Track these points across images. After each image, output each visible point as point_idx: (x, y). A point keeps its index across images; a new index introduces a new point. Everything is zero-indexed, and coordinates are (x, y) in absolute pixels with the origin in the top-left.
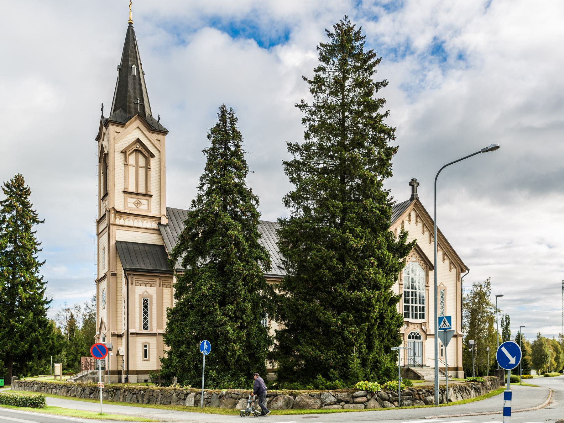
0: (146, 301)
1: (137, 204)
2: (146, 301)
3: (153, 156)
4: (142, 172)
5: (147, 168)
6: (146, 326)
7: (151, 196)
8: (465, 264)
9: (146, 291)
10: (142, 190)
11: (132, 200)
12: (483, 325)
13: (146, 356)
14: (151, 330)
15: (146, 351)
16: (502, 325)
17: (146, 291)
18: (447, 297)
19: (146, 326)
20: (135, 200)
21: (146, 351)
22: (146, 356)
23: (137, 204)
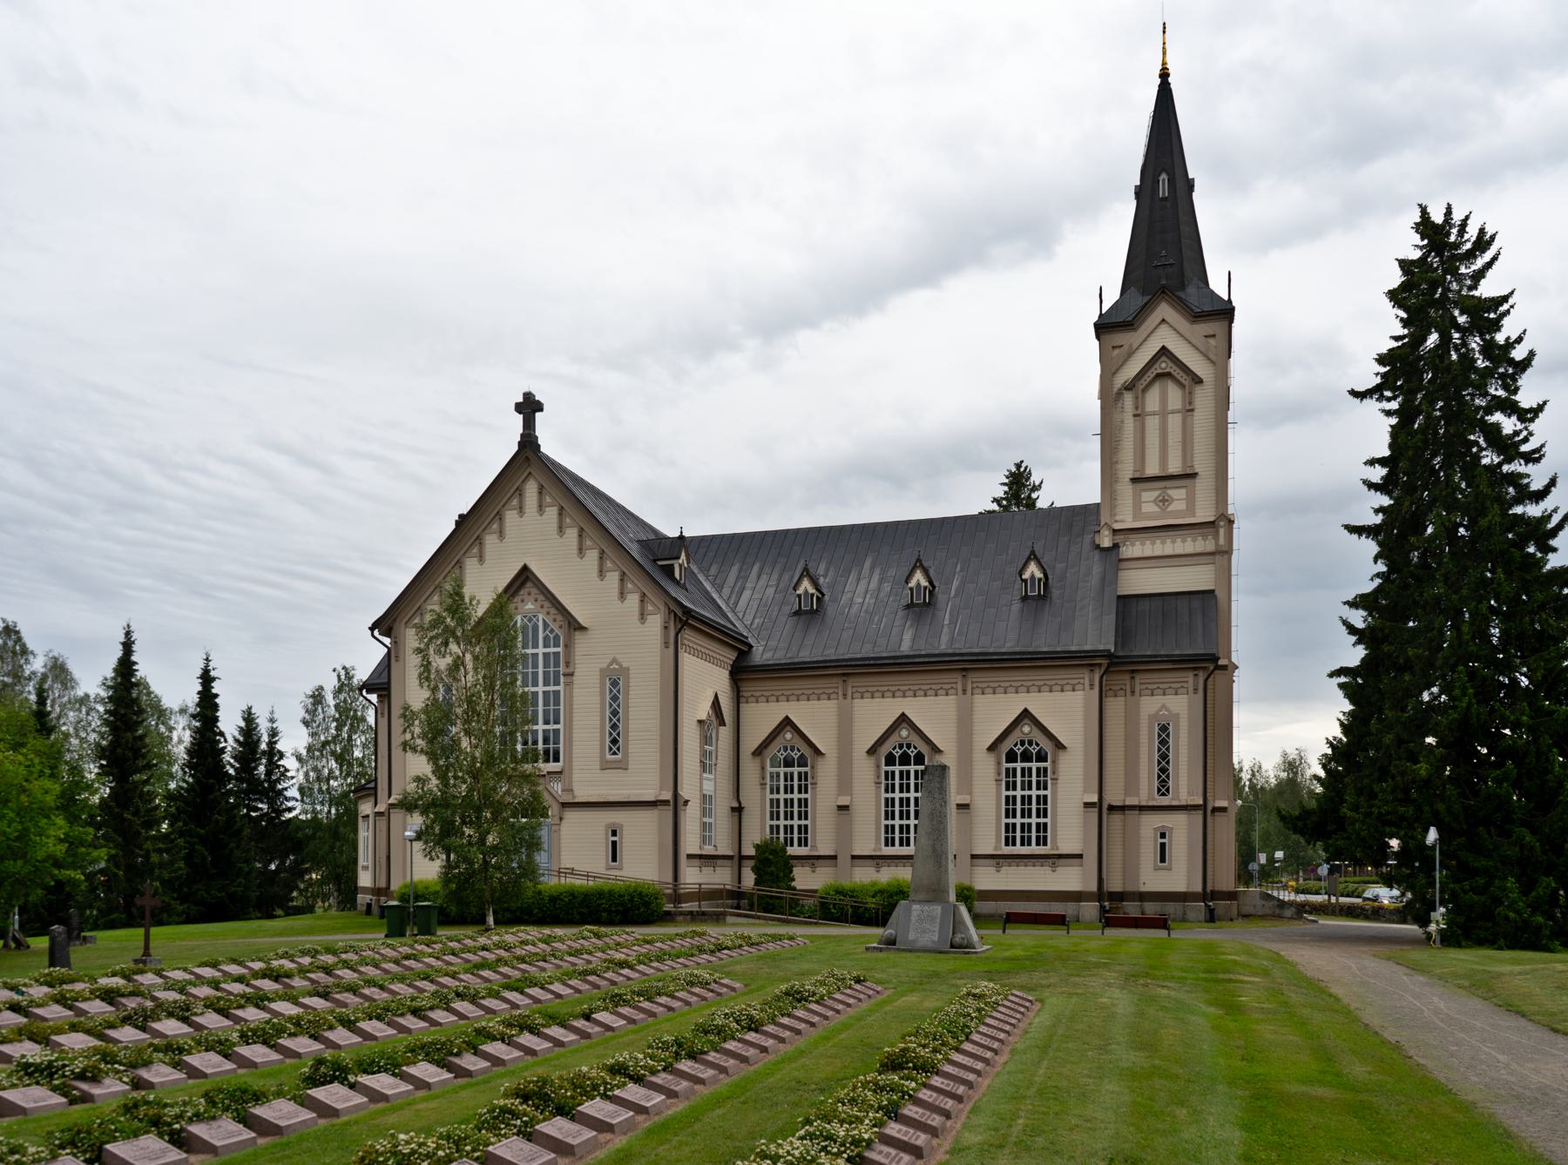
0: (1164, 728)
1: (1164, 501)
2: (1164, 728)
3: (1198, 381)
4: (1175, 422)
5: (1189, 410)
6: (1163, 788)
7: (1193, 476)
8: (618, 500)
9: (1164, 707)
10: (1174, 467)
11: (1149, 495)
12: (1550, 777)
13: (1163, 860)
14: (814, 847)
15: (1163, 846)
16: (718, 918)
17: (1164, 707)
18: (632, 725)
19: (1163, 788)
20: (1156, 493)
21: (1163, 846)
22: (1163, 860)
23: (1164, 501)
